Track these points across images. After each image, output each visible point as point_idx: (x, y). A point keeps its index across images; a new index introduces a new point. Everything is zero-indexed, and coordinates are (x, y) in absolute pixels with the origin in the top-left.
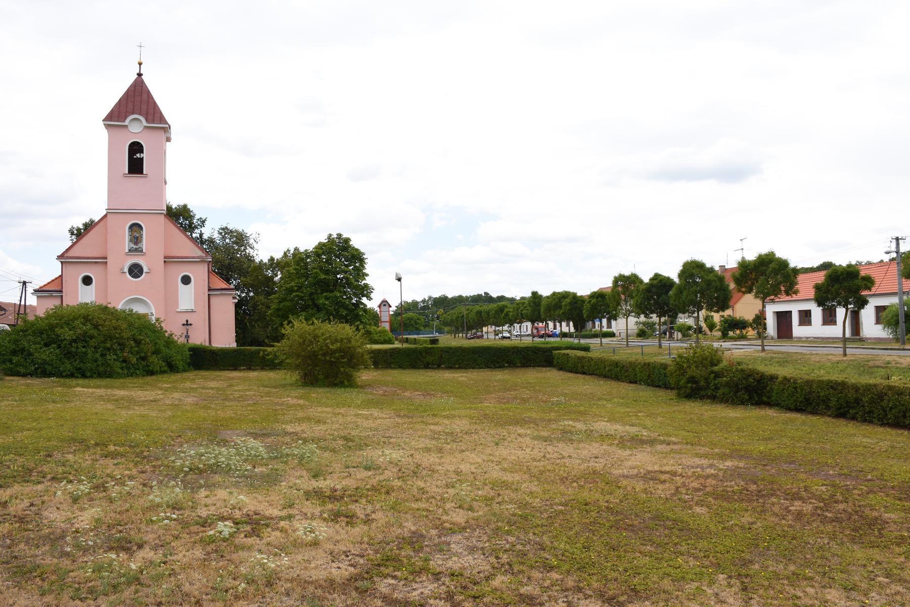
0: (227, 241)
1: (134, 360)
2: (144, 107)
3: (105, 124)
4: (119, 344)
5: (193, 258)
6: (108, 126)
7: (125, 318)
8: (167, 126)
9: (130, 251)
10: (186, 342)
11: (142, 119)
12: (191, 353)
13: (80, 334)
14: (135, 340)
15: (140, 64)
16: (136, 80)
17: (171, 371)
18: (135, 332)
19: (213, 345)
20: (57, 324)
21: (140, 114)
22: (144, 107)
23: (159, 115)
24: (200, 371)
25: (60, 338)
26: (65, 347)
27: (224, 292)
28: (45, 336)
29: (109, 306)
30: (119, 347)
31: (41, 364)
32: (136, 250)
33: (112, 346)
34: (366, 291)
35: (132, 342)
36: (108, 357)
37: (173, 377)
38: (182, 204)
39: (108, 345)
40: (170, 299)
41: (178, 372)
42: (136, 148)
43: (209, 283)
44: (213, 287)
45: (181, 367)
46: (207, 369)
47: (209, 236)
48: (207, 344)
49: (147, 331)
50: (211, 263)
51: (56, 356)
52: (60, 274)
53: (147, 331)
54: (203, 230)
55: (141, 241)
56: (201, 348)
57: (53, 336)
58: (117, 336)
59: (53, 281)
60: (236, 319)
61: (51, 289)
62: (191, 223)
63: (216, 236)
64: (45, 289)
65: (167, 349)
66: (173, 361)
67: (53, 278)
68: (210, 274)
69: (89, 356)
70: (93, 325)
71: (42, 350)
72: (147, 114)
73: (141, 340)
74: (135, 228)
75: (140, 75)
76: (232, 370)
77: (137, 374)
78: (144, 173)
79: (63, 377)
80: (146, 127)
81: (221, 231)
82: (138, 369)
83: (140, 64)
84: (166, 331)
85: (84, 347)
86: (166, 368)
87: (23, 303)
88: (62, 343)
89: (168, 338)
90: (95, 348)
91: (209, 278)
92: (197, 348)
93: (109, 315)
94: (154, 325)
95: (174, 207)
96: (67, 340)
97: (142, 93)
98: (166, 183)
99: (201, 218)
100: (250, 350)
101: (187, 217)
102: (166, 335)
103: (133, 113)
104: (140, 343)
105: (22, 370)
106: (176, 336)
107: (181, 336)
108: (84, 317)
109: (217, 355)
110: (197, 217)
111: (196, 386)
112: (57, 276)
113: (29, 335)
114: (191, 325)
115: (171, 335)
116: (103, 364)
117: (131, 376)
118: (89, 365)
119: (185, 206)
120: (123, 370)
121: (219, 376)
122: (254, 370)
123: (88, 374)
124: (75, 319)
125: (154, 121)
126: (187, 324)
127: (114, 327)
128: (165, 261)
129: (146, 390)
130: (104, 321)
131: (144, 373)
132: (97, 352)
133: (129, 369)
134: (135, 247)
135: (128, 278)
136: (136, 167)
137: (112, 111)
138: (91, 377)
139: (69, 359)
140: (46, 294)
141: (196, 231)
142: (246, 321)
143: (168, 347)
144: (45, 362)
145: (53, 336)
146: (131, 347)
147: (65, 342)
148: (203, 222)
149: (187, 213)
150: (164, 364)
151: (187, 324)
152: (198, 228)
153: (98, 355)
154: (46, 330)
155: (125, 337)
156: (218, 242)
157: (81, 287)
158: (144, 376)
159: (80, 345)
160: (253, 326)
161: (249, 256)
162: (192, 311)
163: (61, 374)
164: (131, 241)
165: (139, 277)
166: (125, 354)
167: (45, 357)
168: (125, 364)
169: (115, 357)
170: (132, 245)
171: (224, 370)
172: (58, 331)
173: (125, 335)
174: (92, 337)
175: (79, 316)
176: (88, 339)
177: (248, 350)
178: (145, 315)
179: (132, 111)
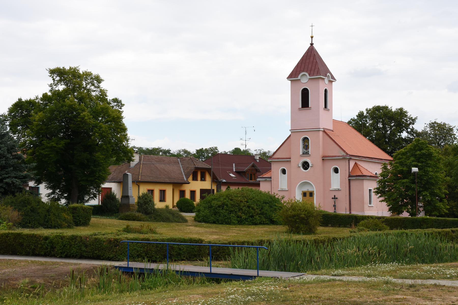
5: (339, 156)
9: (303, 154)
11: (307, 74)
15: (312, 37)
27: (358, 178)
40: (327, 182)
42: (305, 94)
47: (423, 129)
74: (306, 140)
75: (312, 44)
78: (309, 107)
80: (310, 79)
83: (312, 37)
103: (303, 71)
114: (337, 198)
119: (401, 109)
126: (335, 198)
134: (306, 151)
135: (303, 171)
136: (305, 103)
148: (413, 121)
151: (335, 198)
157: (281, 175)
162: (339, 190)
164: (304, 148)
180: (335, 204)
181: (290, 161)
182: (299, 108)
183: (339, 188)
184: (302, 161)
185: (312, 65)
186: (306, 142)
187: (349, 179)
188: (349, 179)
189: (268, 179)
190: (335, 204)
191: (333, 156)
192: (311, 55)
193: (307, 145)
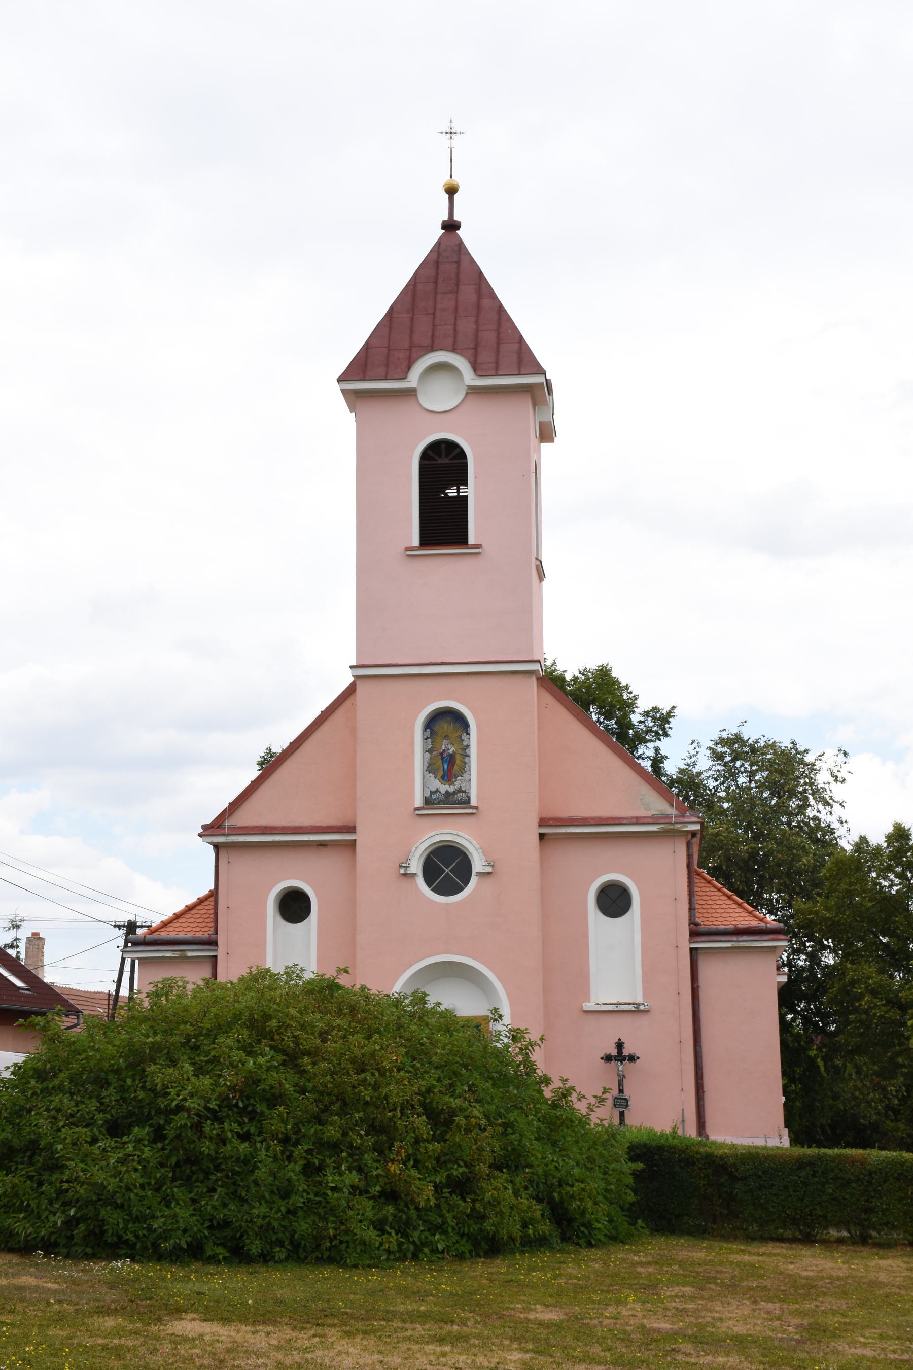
0: (742, 780)
1: (426, 1194)
2: (466, 326)
3: (344, 392)
4: (373, 1128)
5: (638, 821)
6: (354, 398)
7: (399, 1027)
8: (539, 379)
9: (428, 802)
10: (616, 1121)
11: (460, 362)
12: (640, 1166)
13: (232, 1088)
14: (432, 1113)
15: (451, 191)
16: (439, 244)
17: (564, 1239)
18: (430, 1079)
19: (712, 1138)
20: (154, 1046)
21: (454, 349)
22: (466, 326)
23: (516, 347)
24: (673, 1241)
25: (162, 1103)
26: (178, 1137)
28: (110, 1094)
29: (343, 980)
30: (370, 1141)
31: (88, 1202)
32: (449, 799)
33: (345, 1134)
34: (657, 1132)
35: (420, 1122)
36: (331, 1179)
37: (571, 1269)
38: (593, 664)
39: (332, 1132)
41: (590, 1245)
43: (691, 909)
44: (706, 923)
45: (602, 1225)
46: (699, 1232)
48: (691, 1131)
49: (476, 1078)
50: (696, 841)
51: (145, 1172)
52: (212, 887)
53: (476, 1078)
54: (665, 745)
55: (464, 769)
56: (672, 1149)
57: (141, 1094)
58: (367, 1094)
59: (189, 909)
60: (783, 1044)
61: (181, 936)
62: (624, 724)
63: (704, 764)
64: (164, 935)
65: (549, 1148)
66: (572, 1197)
67: (191, 900)
68: (697, 880)
69: (261, 1173)
70: (283, 1052)
71: (96, 1150)
72: (476, 349)
73: (453, 1113)
74: (445, 726)
75: (451, 226)
76: (793, 1240)
77: (435, 1251)
78: (471, 541)
79: (159, 1257)
80: (474, 391)
81: (719, 749)
82: (441, 1228)
83: (451, 191)
84: (547, 1081)
85: (245, 1137)
86: (545, 1228)
87: (124, 992)
88: (169, 1122)
89: (555, 1106)
90: (285, 1140)
91: (691, 894)
92: (661, 1149)
93: (340, 1013)
94: (500, 1055)
95: (568, 677)
96: (188, 1110)
97: (457, 285)
98: (541, 576)
99: (655, 709)
100: (863, 1162)
101: (612, 706)
102: (547, 1093)
103: (432, 348)
104: (449, 1123)
105: (21, 1226)
106: (581, 1097)
107: (601, 1101)
108: (252, 1024)
109: (733, 1178)
110: (643, 705)
111: (665, 1326)
112: (204, 892)
113: (60, 1089)
114: (632, 1058)
115: (565, 1094)
116: (309, 1207)
117: (415, 1257)
118: (259, 1210)
119: (604, 673)
120: (383, 1232)
121: (752, 1271)
122: (885, 1246)
123: (255, 1247)
124: (221, 1028)
125: (497, 368)
127: (353, 1061)
128: (542, 836)
129: (456, 1339)
130: (323, 1036)
131: (465, 1246)
132: (289, 1158)
133: (403, 1229)
134: (444, 788)
137: (367, 347)
138: (265, 1258)
139: (188, 1182)
140: (166, 953)
141: (641, 749)
142: (812, 1053)
143: (554, 1144)
144: (102, 1197)
145: (141, 1094)
146: (417, 1141)
147: (181, 1120)
149: (612, 693)
150: (537, 1210)
152: (646, 741)
153: (293, 1170)
154: (117, 1072)
155: (393, 1099)
156: (712, 784)
158: (461, 1257)
159: (230, 1127)
160: (838, 1071)
161: (818, 827)
162: (637, 1010)
163: (155, 1246)
164: (430, 768)
165: (456, 890)
166: (393, 1167)
167: (100, 1177)
168: (391, 1209)
169: (353, 1178)
170: (436, 784)
171: (764, 1239)
172: (158, 1073)
173: (395, 1092)
174: (274, 1099)
175: (237, 1017)
176: (261, 1107)
177: (853, 1161)
178: (477, 1026)
179: (428, 342)
180: (621, 1091)
181: (353, 844)
182: (407, 549)
183: (640, 1000)
184: (426, 844)
185: (477, 322)
186: (446, 737)
187: (691, 949)
188: (691, 949)
189: (193, 952)
190: (621, 1091)
191: (600, 819)
192: (458, 274)
193: (452, 757)
